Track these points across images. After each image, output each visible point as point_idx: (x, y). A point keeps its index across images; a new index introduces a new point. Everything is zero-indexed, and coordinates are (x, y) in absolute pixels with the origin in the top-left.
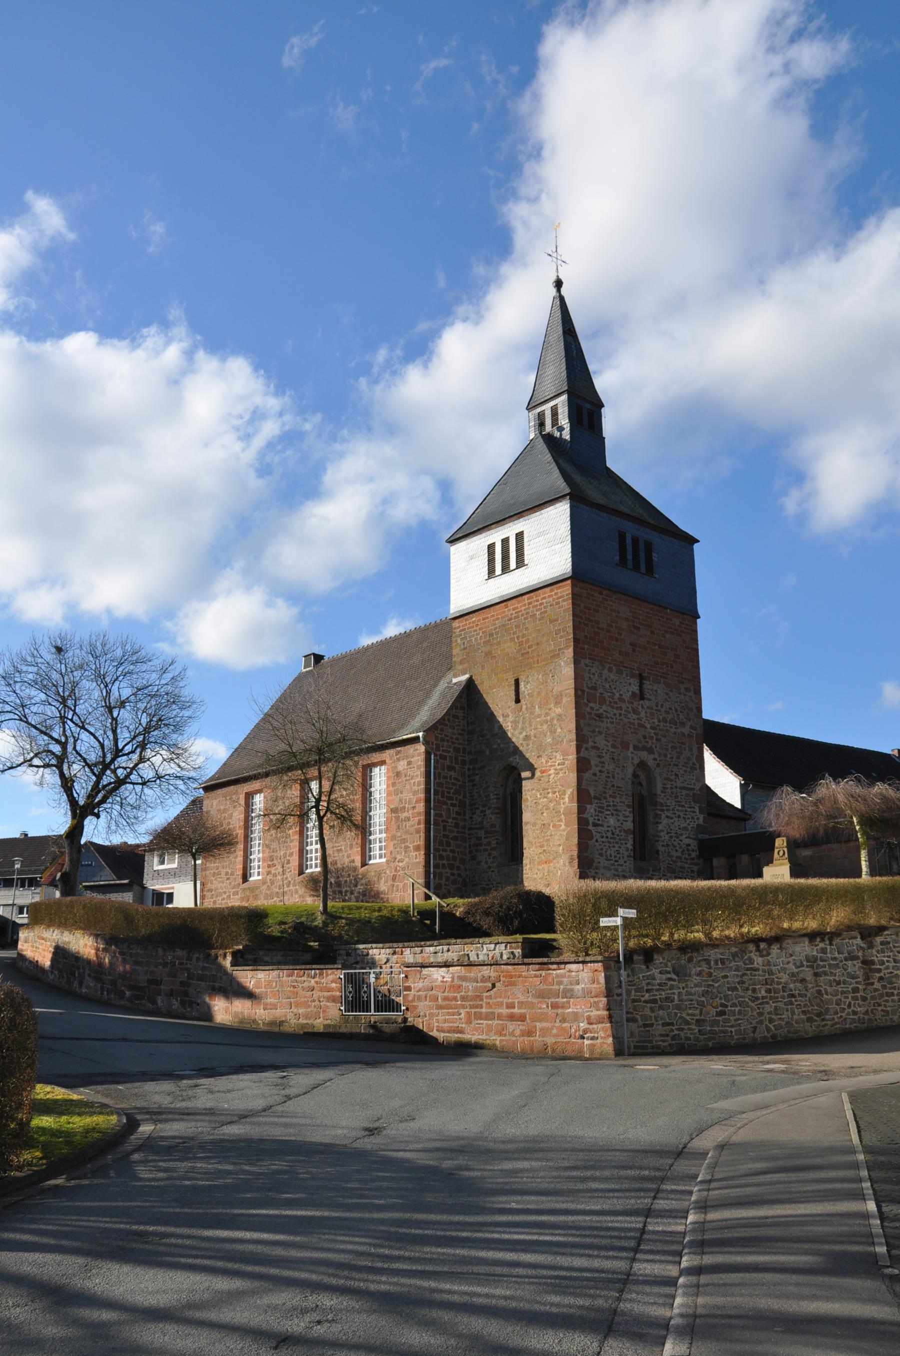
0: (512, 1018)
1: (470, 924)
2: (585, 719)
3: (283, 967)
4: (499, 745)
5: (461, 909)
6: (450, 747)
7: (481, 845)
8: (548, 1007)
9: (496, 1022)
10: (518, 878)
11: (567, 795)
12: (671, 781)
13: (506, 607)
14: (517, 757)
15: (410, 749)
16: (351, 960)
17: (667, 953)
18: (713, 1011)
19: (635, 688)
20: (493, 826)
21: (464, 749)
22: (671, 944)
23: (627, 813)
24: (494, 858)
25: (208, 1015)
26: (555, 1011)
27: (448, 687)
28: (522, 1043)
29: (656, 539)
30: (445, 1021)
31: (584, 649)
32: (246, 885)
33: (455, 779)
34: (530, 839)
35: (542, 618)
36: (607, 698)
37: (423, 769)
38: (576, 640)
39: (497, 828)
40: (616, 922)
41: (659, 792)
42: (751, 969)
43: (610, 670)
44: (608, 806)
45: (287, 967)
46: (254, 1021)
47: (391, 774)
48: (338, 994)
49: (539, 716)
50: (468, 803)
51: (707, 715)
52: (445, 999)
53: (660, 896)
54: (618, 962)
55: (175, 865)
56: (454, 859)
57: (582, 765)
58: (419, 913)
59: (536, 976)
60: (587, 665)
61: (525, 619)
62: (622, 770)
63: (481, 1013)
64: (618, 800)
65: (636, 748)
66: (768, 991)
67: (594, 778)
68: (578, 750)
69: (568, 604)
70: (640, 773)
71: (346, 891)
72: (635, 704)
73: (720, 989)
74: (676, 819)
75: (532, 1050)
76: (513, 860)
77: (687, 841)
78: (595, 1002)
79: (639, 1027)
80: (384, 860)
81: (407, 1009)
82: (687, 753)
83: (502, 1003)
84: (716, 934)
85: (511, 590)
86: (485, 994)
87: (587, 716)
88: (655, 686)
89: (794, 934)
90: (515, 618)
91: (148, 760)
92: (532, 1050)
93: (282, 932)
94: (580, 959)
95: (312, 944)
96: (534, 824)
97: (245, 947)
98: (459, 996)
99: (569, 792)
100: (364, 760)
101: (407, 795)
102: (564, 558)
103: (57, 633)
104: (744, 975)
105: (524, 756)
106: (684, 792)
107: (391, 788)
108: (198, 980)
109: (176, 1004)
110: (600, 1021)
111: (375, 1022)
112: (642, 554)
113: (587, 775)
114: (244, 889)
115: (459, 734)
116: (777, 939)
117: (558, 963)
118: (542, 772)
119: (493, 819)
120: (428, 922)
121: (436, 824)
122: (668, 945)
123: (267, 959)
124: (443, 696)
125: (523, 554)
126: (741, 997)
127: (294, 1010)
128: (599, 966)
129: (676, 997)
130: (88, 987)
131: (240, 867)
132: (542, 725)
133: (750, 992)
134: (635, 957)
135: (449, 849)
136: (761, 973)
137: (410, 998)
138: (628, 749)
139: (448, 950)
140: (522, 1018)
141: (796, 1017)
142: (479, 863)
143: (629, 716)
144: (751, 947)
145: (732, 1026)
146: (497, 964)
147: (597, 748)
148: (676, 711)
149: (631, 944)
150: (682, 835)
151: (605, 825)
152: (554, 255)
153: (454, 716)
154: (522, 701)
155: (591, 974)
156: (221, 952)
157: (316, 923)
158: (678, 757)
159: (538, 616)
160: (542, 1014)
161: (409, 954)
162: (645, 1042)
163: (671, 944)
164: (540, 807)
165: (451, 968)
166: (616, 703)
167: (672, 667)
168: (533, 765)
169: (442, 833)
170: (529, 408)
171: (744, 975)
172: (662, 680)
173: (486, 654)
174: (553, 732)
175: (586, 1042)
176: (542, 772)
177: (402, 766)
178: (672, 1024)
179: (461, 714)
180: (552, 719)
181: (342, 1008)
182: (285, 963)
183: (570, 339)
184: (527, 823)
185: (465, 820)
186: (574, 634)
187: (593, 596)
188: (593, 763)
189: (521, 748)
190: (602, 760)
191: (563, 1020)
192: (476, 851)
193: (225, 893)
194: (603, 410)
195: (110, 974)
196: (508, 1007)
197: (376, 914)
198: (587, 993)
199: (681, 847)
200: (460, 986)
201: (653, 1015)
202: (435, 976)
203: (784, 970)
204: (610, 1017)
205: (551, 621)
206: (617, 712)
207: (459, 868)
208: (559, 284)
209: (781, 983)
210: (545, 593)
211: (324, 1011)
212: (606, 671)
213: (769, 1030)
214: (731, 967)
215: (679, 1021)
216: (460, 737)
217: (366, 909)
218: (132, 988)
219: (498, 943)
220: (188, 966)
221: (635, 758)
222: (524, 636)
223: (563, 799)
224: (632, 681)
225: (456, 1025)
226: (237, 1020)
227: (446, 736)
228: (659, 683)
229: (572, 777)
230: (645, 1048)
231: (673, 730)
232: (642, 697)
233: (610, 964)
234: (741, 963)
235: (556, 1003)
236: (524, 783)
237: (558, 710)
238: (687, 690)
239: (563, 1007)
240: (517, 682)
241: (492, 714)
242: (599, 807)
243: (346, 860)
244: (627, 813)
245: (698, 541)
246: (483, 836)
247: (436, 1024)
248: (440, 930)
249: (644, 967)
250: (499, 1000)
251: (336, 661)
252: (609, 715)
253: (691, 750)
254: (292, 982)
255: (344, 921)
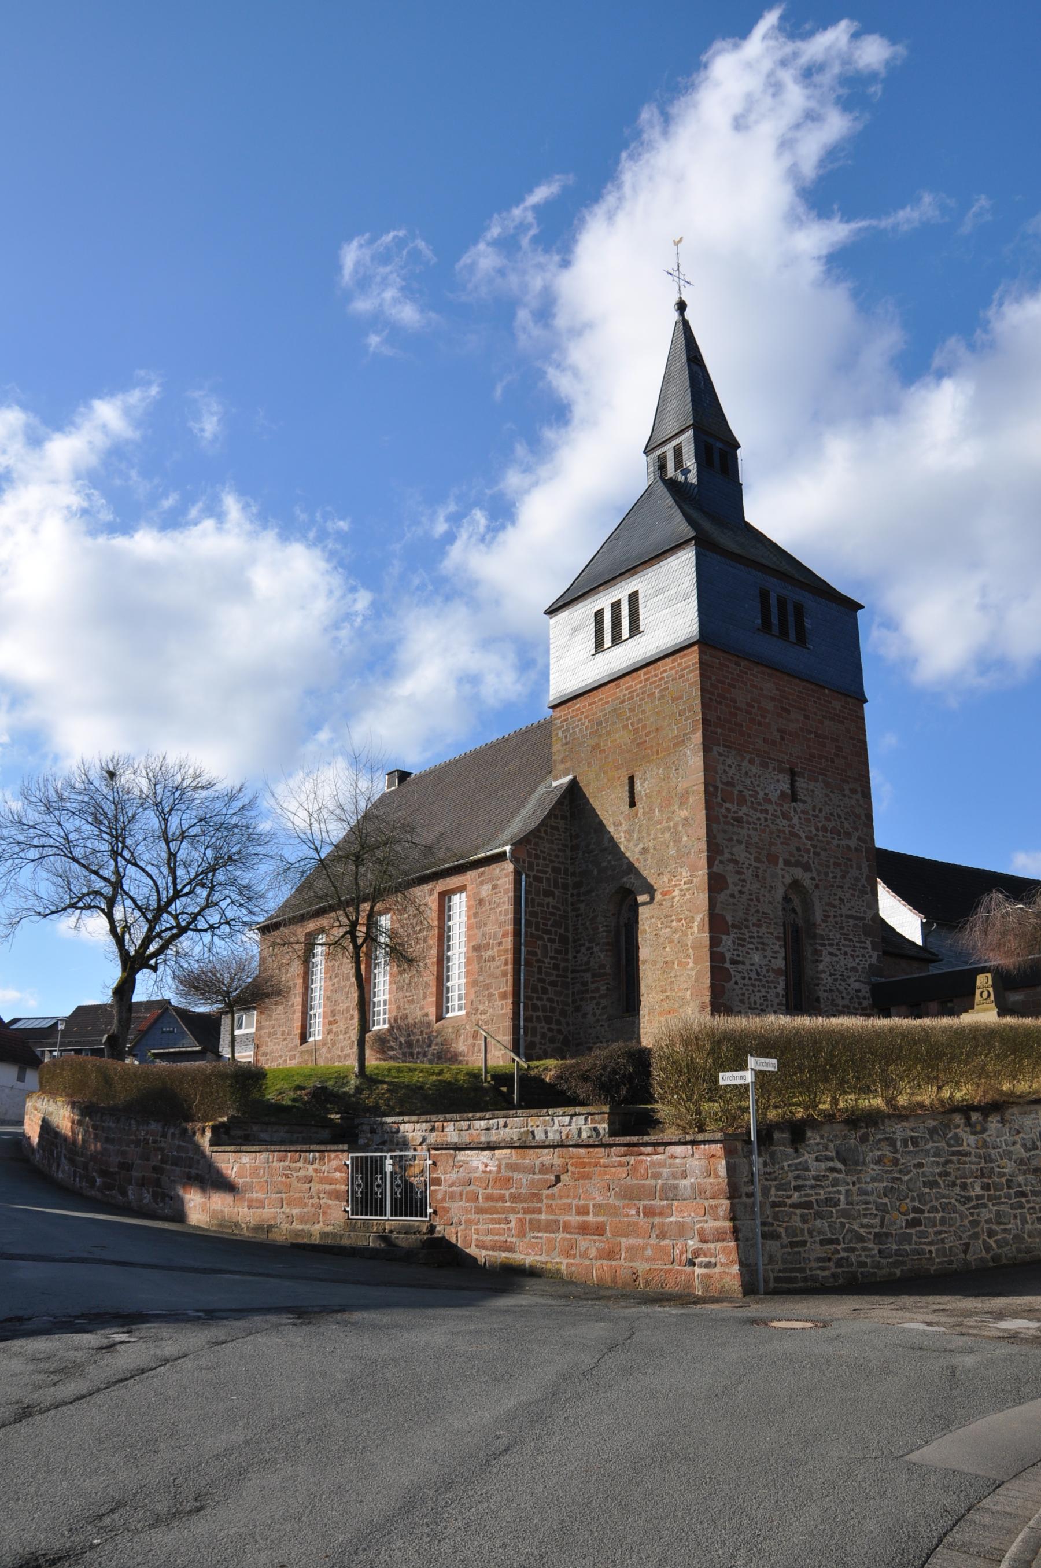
0: (584, 1229)
1: (563, 1093)
2: (719, 823)
3: (273, 1148)
4: (609, 862)
5: (552, 1073)
6: (547, 866)
7: (587, 991)
8: (638, 1213)
9: (561, 1235)
10: (632, 1029)
11: (696, 923)
12: (835, 907)
13: (618, 686)
14: (632, 876)
15: (495, 869)
16: (377, 1138)
17: (827, 1128)
18: (902, 1220)
19: (785, 787)
20: (602, 966)
21: (566, 870)
22: (833, 1116)
23: (776, 948)
24: (603, 1008)
25: (180, 1216)
26: (650, 1220)
27: (547, 792)
28: (598, 1270)
29: (810, 602)
30: (488, 1232)
31: (716, 733)
32: (304, 1047)
33: (554, 907)
34: (650, 982)
35: (663, 697)
36: (748, 797)
37: (511, 894)
38: (705, 721)
39: (608, 970)
40: (744, 1078)
41: (818, 921)
42: (959, 1153)
43: (751, 762)
44: (751, 937)
45: (278, 1148)
46: (237, 1224)
47: (472, 903)
48: (343, 1188)
49: (660, 822)
50: (570, 939)
51: (877, 846)
52: (489, 1198)
53: (815, 1041)
54: (749, 1142)
55: (253, 1030)
56: (553, 1010)
57: (716, 883)
58: (493, 1077)
59: (621, 1165)
60: (720, 755)
61: (641, 700)
62: (770, 891)
63: (539, 1221)
64: (764, 930)
65: (787, 863)
66: (986, 1187)
67: (731, 900)
68: (709, 868)
69: (694, 676)
70: (793, 896)
71: (418, 1053)
72: (786, 807)
73: (911, 1186)
74: (842, 957)
75: (614, 1281)
76: (627, 1011)
77: (857, 985)
78: (711, 1207)
79: (782, 1247)
80: (463, 1012)
81: (435, 1212)
82: (854, 873)
83: (569, 1205)
84: (902, 1100)
85: (624, 666)
86: (545, 1192)
87: (722, 819)
88: (812, 785)
89: (1021, 1100)
90: (629, 699)
91: (216, 904)
92: (614, 1281)
93: (294, 1100)
94: (688, 1138)
95: (332, 1116)
96: (654, 963)
97: (232, 1119)
98: (507, 1193)
99: (698, 918)
100: (442, 885)
101: (492, 928)
102: (690, 618)
103: (110, 755)
104: (948, 1162)
105: (640, 874)
106: (852, 922)
107: (473, 920)
108: (172, 1165)
109: (147, 1197)
110: (719, 1237)
111: (391, 1231)
112: (791, 619)
113: (722, 897)
114: (302, 1052)
115: (559, 850)
116: (997, 1107)
117: (655, 1145)
118: (664, 894)
119: (602, 957)
120: (504, 1089)
121: (528, 964)
122: (830, 1117)
123: (263, 1136)
124: (541, 801)
125: (638, 619)
126: (944, 1197)
127: (286, 1209)
128: (717, 1149)
129: (842, 1198)
130: (63, 1171)
131: (298, 1024)
132: (663, 833)
133: (957, 1190)
134: (777, 1135)
135: (545, 997)
136: (974, 1159)
137: (440, 1196)
138: (777, 864)
139: (505, 1126)
140: (599, 1230)
141: (1028, 1227)
142: (585, 1015)
143: (778, 821)
144: (958, 1119)
145: (931, 1243)
146: (562, 1146)
147: (736, 862)
148: (840, 817)
149: (772, 1115)
150: (849, 977)
151: (748, 962)
152: (676, 273)
153: (552, 827)
154: (639, 805)
155: (704, 1162)
156: (199, 1125)
157: (346, 1089)
158: (843, 877)
159: (657, 695)
160: (630, 1224)
161: (452, 1132)
162: (792, 1270)
163: (833, 1116)
164: (661, 940)
165: (497, 1152)
166: (760, 804)
167: (833, 762)
168: (651, 886)
169: (536, 976)
170: (647, 451)
171: (948, 1162)
172: (820, 777)
173: (593, 748)
174: (678, 841)
175: (698, 1271)
176: (664, 894)
177: (485, 891)
178: (836, 1241)
179: (561, 824)
180: (676, 825)
181: (348, 1209)
182: (292, 1142)
183: (696, 368)
184: (645, 962)
185: (567, 960)
186: (703, 714)
187: (728, 667)
188: (729, 880)
189: (637, 865)
190: (743, 877)
191: (662, 1236)
192: (582, 999)
193: (281, 1056)
194: (739, 451)
195: (83, 1155)
196: (578, 1213)
197: (435, 1078)
198: (698, 1192)
199: (848, 994)
200: (509, 1180)
201: (806, 1226)
202: (475, 1164)
203: (1009, 1154)
204: (735, 1231)
205: (673, 701)
206: (762, 816)
207: (558, 1022)
208: (682, 306)
209: (1004, 1175)
210: (666, 665)
211: (324, 1213)
212: (745, 764)
213: (988, 1248)
214: (927, 1151)
215: (849, 1236)
216: (560, 854)
217: (421, 1071)
218: (104, 1173)
219: (575, 1115)
220: (163, 1145)
221: (787, 876)
222: (640, 721)
223: (691, 928)
224: (781, 776)
225: (503, 1238)
226: (215, 1222)
227: (542, 851)
228: (817, 781)
229: (703, 898)
230: (793, 1280)
231: (835, 842)
232: (794, 798)
233: (735, 1145)
234: (942, 1144)
235: (652, 1207)
236: (641, 909)
237: (684, 813)
238: (853, 791)
239: (661, 1214)
240: (631, 780)
241: (601, 824)
242: (739, 939)
243: (419, 1013)
244: (776, 948)
245: (862, 607)
246: (590, 980)
247: (475, 1237)
248: (520, 1099)
249: (790, 1150)
250: (565, 1201)
251: (423, 777)
252: (750, 820)
253: (859, 868)
254: (284, 1169)
255: (385, 1086)
